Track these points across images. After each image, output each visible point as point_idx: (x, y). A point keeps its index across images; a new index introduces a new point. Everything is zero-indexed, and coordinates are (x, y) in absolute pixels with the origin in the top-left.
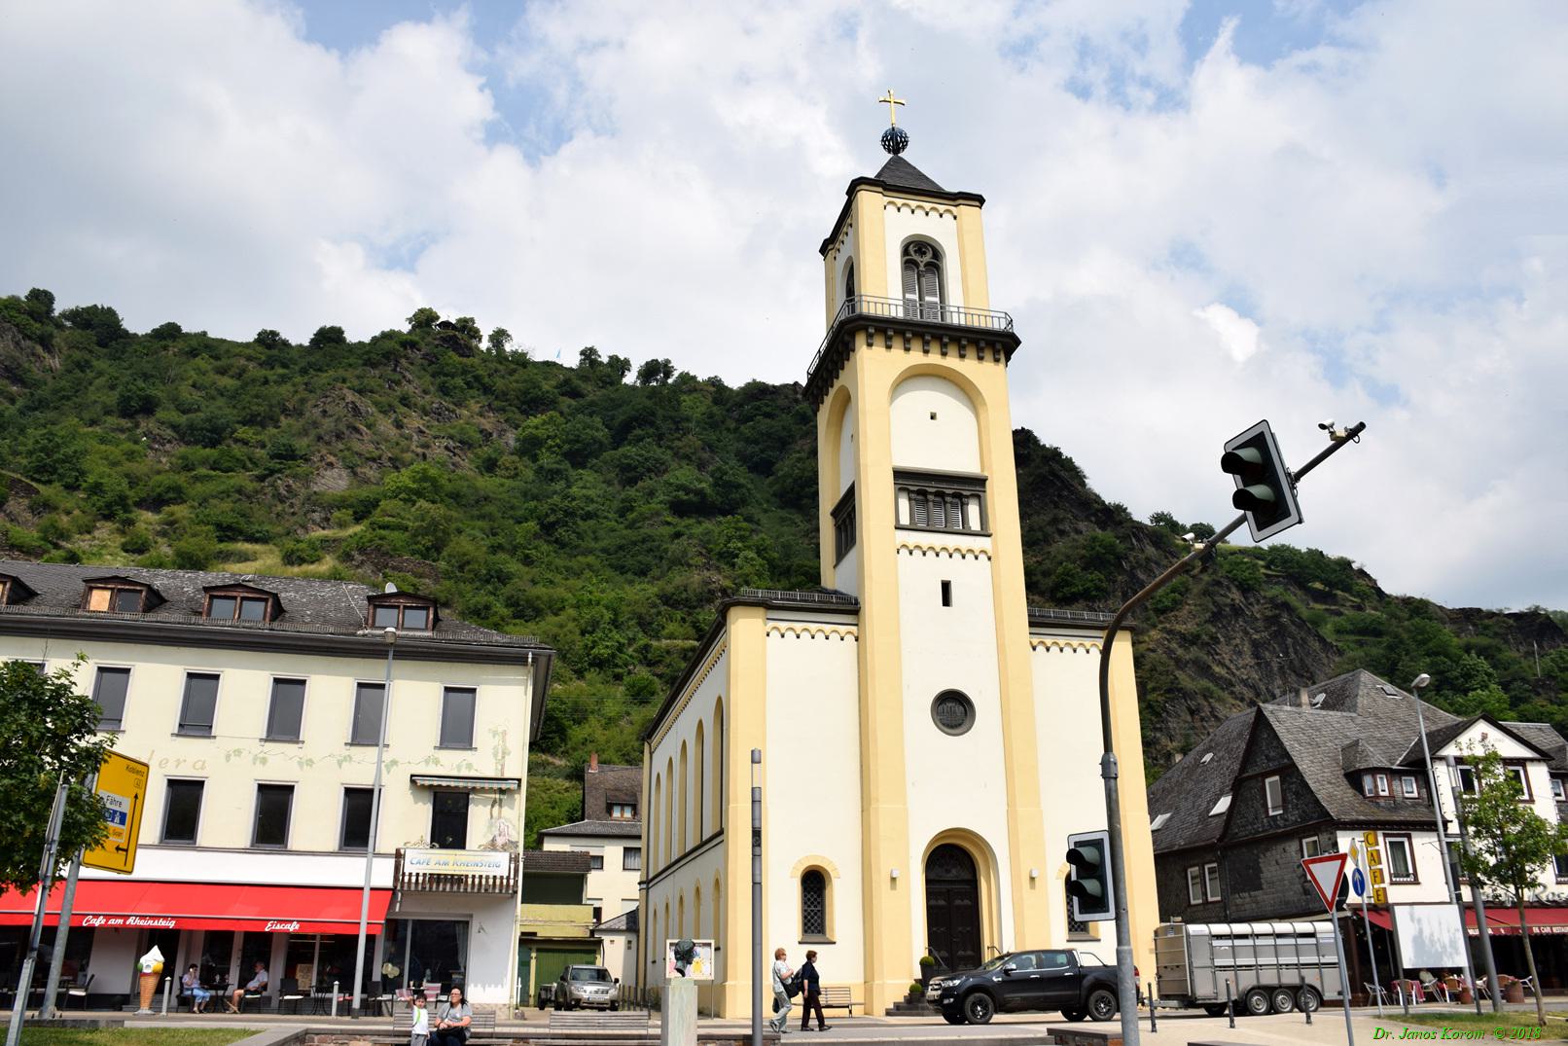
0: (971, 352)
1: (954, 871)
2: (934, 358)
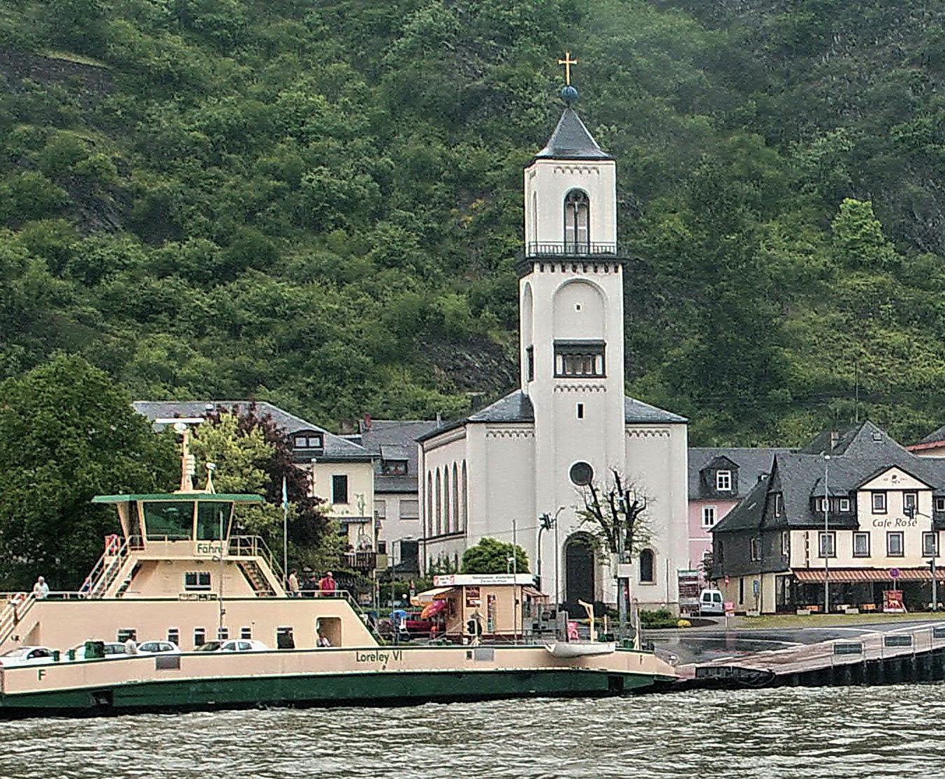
0: (601, 270)
2: (581, 275)
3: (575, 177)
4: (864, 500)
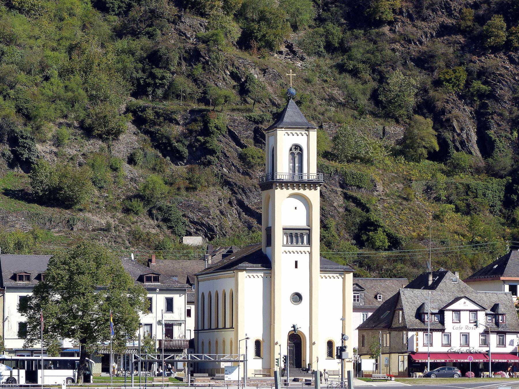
1: (296, 340)
2: (296, 191)
3: (299, 138)
4: (448, 315)
